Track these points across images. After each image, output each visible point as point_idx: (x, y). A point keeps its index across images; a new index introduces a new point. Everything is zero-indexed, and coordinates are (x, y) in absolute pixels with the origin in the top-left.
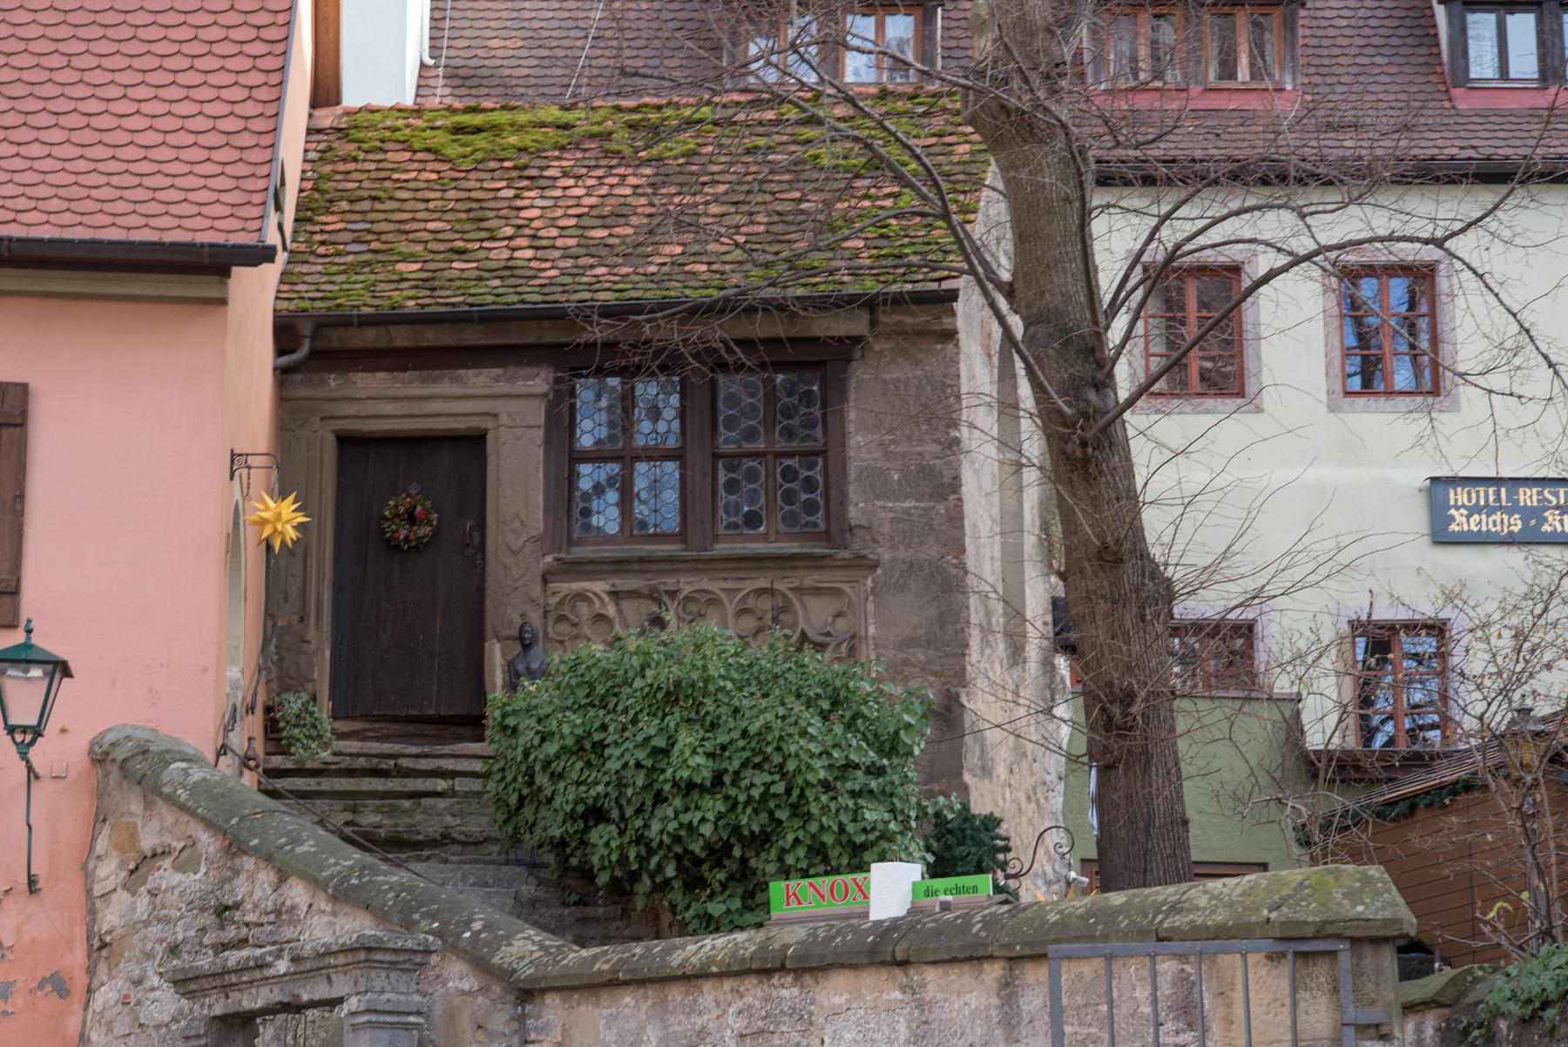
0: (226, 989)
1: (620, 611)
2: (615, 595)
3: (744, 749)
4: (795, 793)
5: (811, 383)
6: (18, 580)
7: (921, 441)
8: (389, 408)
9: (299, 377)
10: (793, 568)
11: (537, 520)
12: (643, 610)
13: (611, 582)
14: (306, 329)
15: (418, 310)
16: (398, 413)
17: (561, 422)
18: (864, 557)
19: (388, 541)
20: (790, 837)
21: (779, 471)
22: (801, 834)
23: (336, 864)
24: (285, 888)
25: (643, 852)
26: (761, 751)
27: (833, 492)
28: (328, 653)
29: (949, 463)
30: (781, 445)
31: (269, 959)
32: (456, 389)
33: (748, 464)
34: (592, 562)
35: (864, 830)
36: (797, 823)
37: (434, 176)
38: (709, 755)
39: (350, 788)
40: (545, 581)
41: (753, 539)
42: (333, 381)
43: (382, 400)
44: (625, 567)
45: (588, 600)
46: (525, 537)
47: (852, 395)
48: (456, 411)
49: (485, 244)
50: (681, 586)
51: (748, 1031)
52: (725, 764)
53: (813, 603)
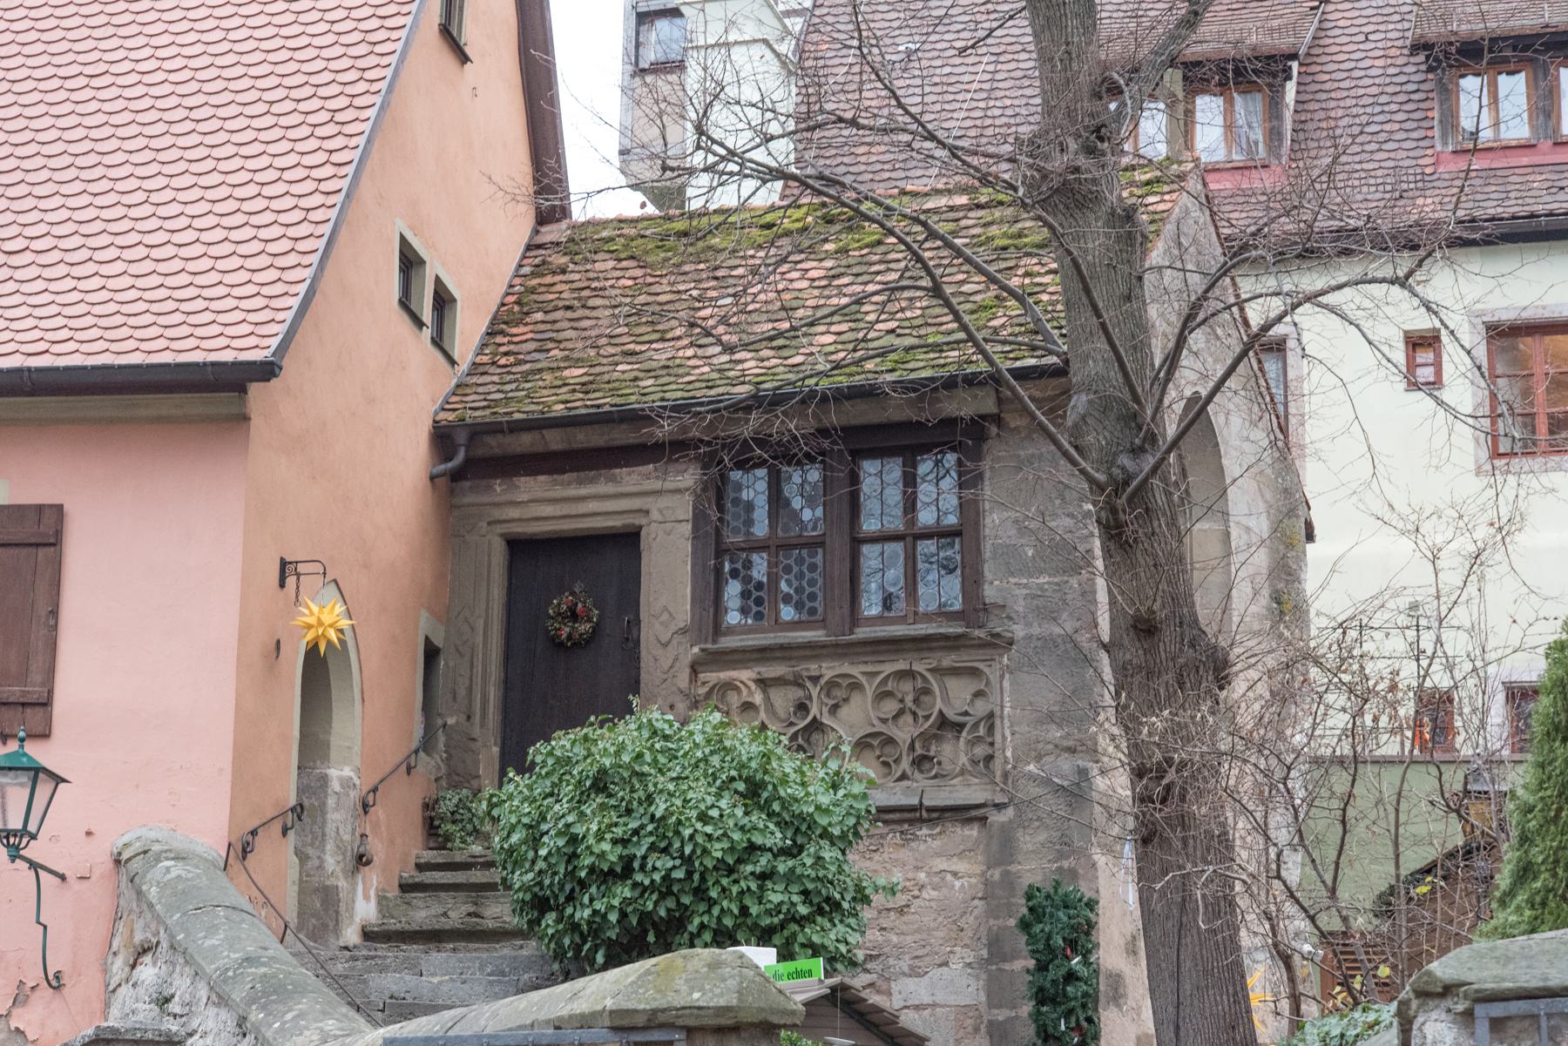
1: (767, 699)
2: (762, 683)
3: (651, 833)
4: (696, 877)
6: (50, 692)
8: (548, 510)
9: (467, 484)
10: (930, 649)
11: (684, 612)
13: (757, 669)
14: (461, 437)
15: (565, 413)
16: (558, 513)
19: (553, 639)
20: (696, 921)
22: (706, 919)
25: (577, 939)
26: (665, 837)
32: (610, 488)
35: (769, 913)
36: (702, 907)
37: (630, 283)
38: (615, 842)
39: (484, 880)
42: (498, 486)
45: (737, 689)
46: (673, 628)
48: (610, 509)
49: (654, 346)
50: (824, 671)
52: (633, 850)
53: (952, 683)
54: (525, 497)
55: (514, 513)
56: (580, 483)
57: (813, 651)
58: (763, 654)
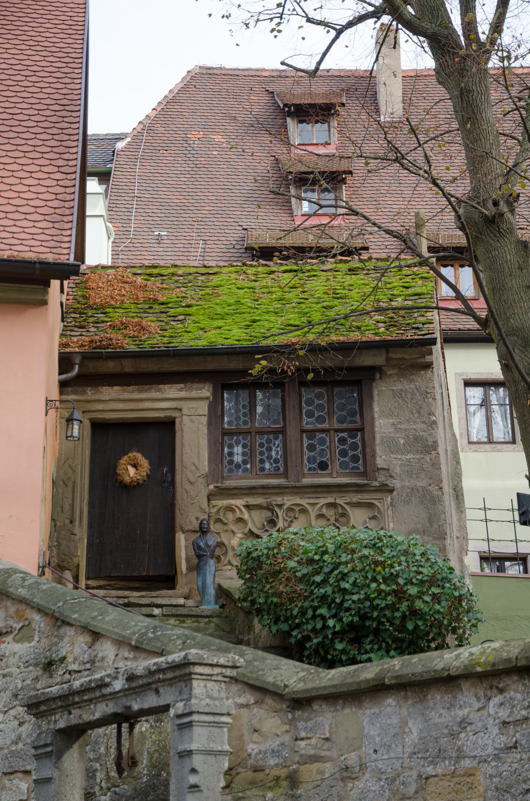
0: (67, 708)
1: (250, 516)
2: (248, 507)
5: (352, 392)
7: (415, 422)
9: (70, 389)
10: (347, 492)
11: (204, 466)
12: (263, 516)
13: (245, 500)
16: (126, 408)
17: (215, 413)
18: (387, 485)
21: (336, 439)
23: (136, 625)
24: (97, 646)
27: (368, 450)
28: (86, 541)
29: (431, 434)
30: (337, 426)
31: (107, 680)
32: (158, 395)
33: (319, 435)
34: (236, 488)
40: (209, 500)
41: (323, 476)
43: (117, 402)
44: (254, 491)
46: (198, 475)
47: (376, 398)
50: (285, 502)
51: (511, 719)
54: (107, 398)
55: (100, 407)
56: (140, 391)
57: (280, 490)
58: (251, 491)
